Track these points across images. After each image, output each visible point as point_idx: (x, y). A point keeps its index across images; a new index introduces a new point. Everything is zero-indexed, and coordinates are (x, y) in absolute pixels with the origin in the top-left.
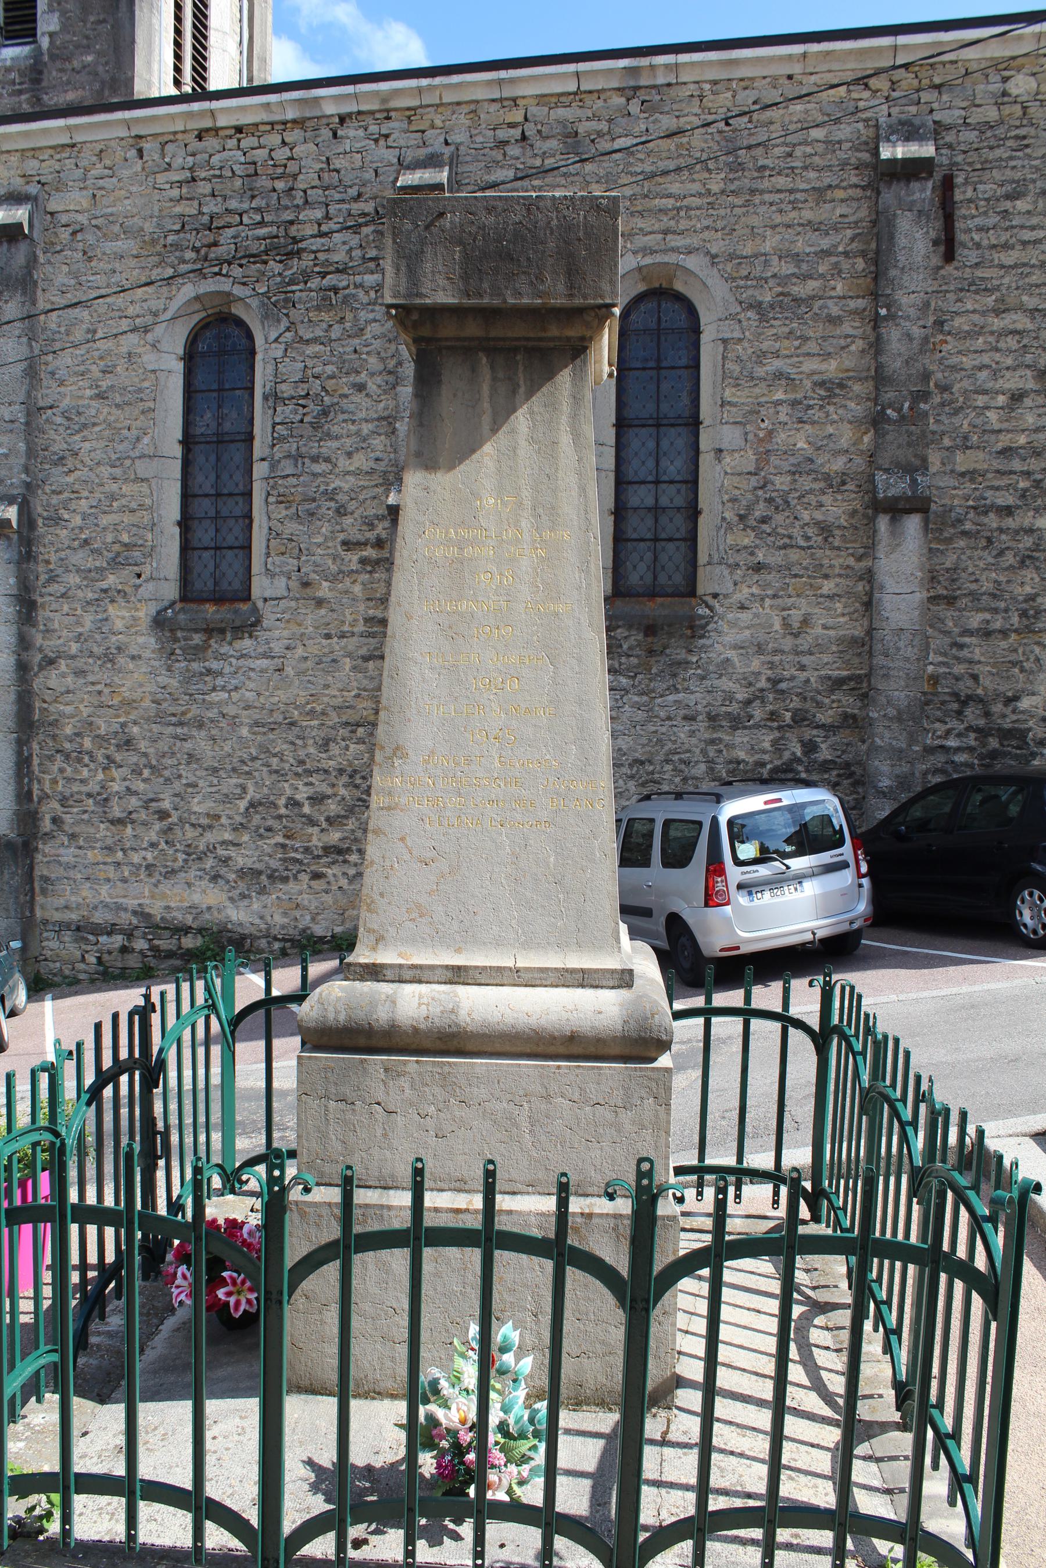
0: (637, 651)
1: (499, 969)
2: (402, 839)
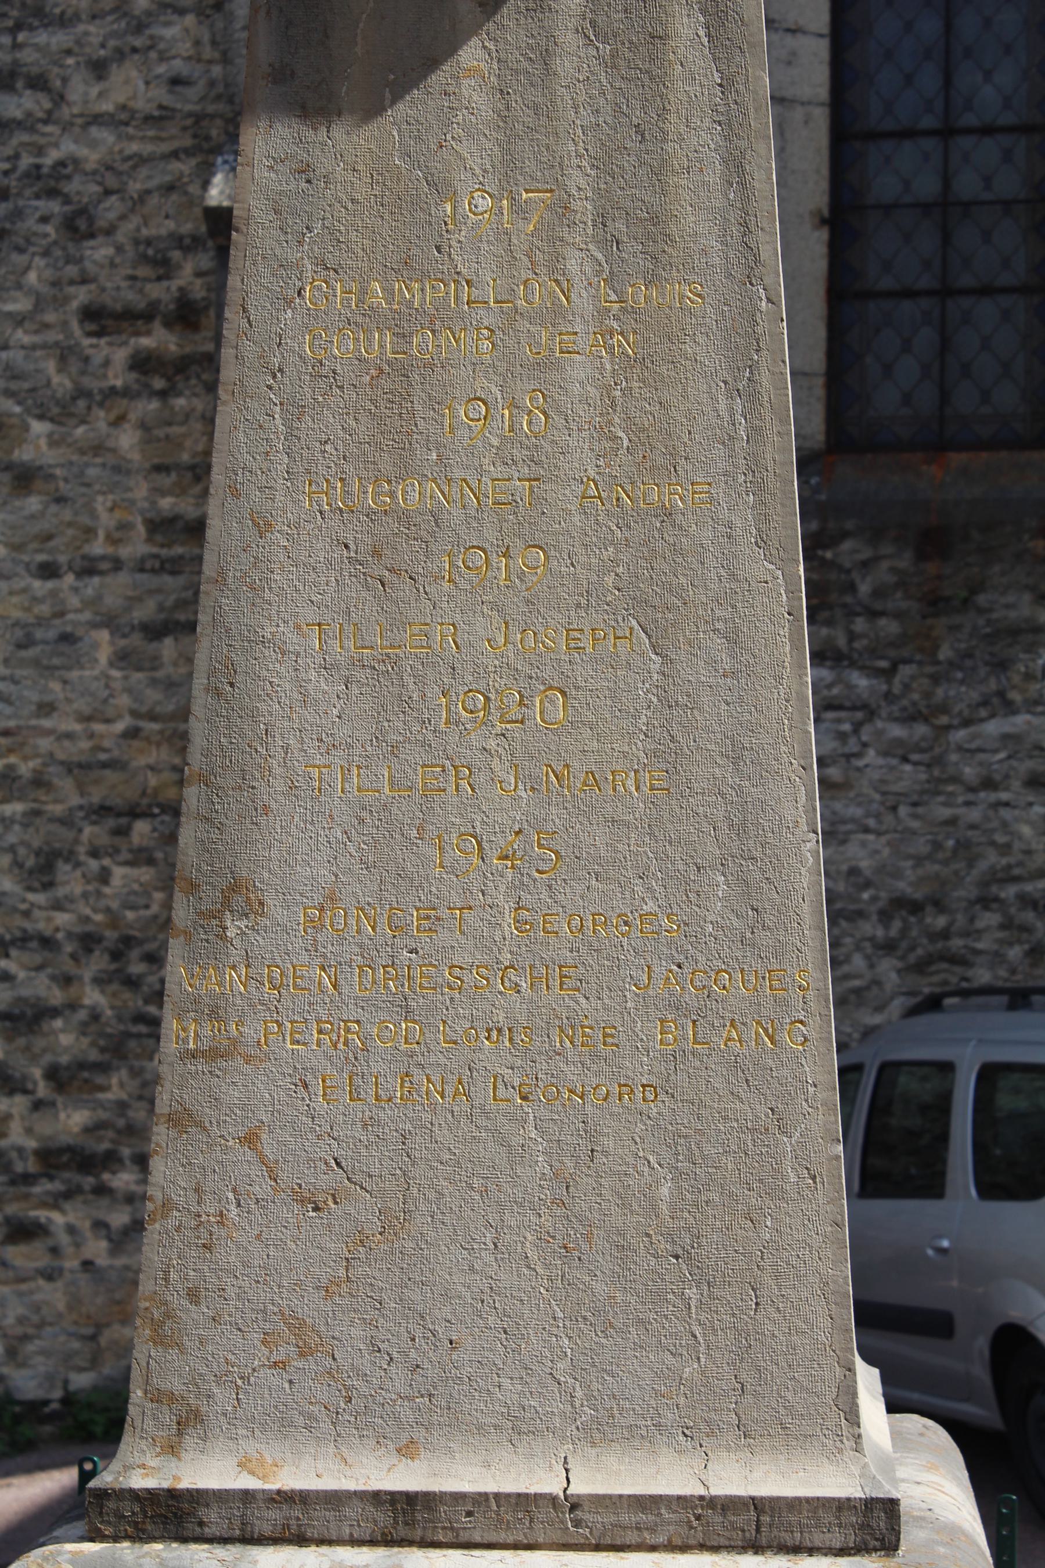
0: (898, 601)
1: (523, 1501)
2: (250, 1140)
